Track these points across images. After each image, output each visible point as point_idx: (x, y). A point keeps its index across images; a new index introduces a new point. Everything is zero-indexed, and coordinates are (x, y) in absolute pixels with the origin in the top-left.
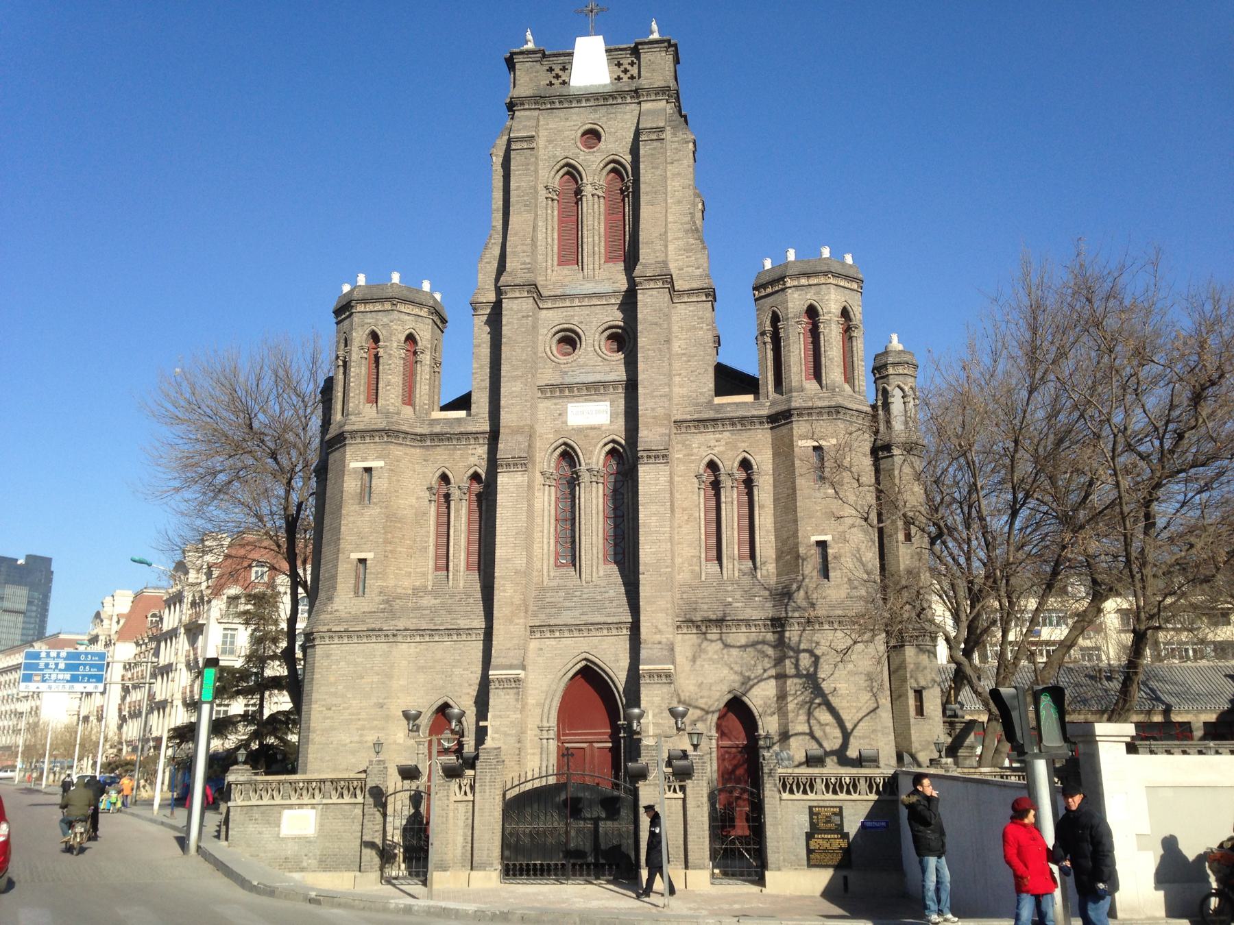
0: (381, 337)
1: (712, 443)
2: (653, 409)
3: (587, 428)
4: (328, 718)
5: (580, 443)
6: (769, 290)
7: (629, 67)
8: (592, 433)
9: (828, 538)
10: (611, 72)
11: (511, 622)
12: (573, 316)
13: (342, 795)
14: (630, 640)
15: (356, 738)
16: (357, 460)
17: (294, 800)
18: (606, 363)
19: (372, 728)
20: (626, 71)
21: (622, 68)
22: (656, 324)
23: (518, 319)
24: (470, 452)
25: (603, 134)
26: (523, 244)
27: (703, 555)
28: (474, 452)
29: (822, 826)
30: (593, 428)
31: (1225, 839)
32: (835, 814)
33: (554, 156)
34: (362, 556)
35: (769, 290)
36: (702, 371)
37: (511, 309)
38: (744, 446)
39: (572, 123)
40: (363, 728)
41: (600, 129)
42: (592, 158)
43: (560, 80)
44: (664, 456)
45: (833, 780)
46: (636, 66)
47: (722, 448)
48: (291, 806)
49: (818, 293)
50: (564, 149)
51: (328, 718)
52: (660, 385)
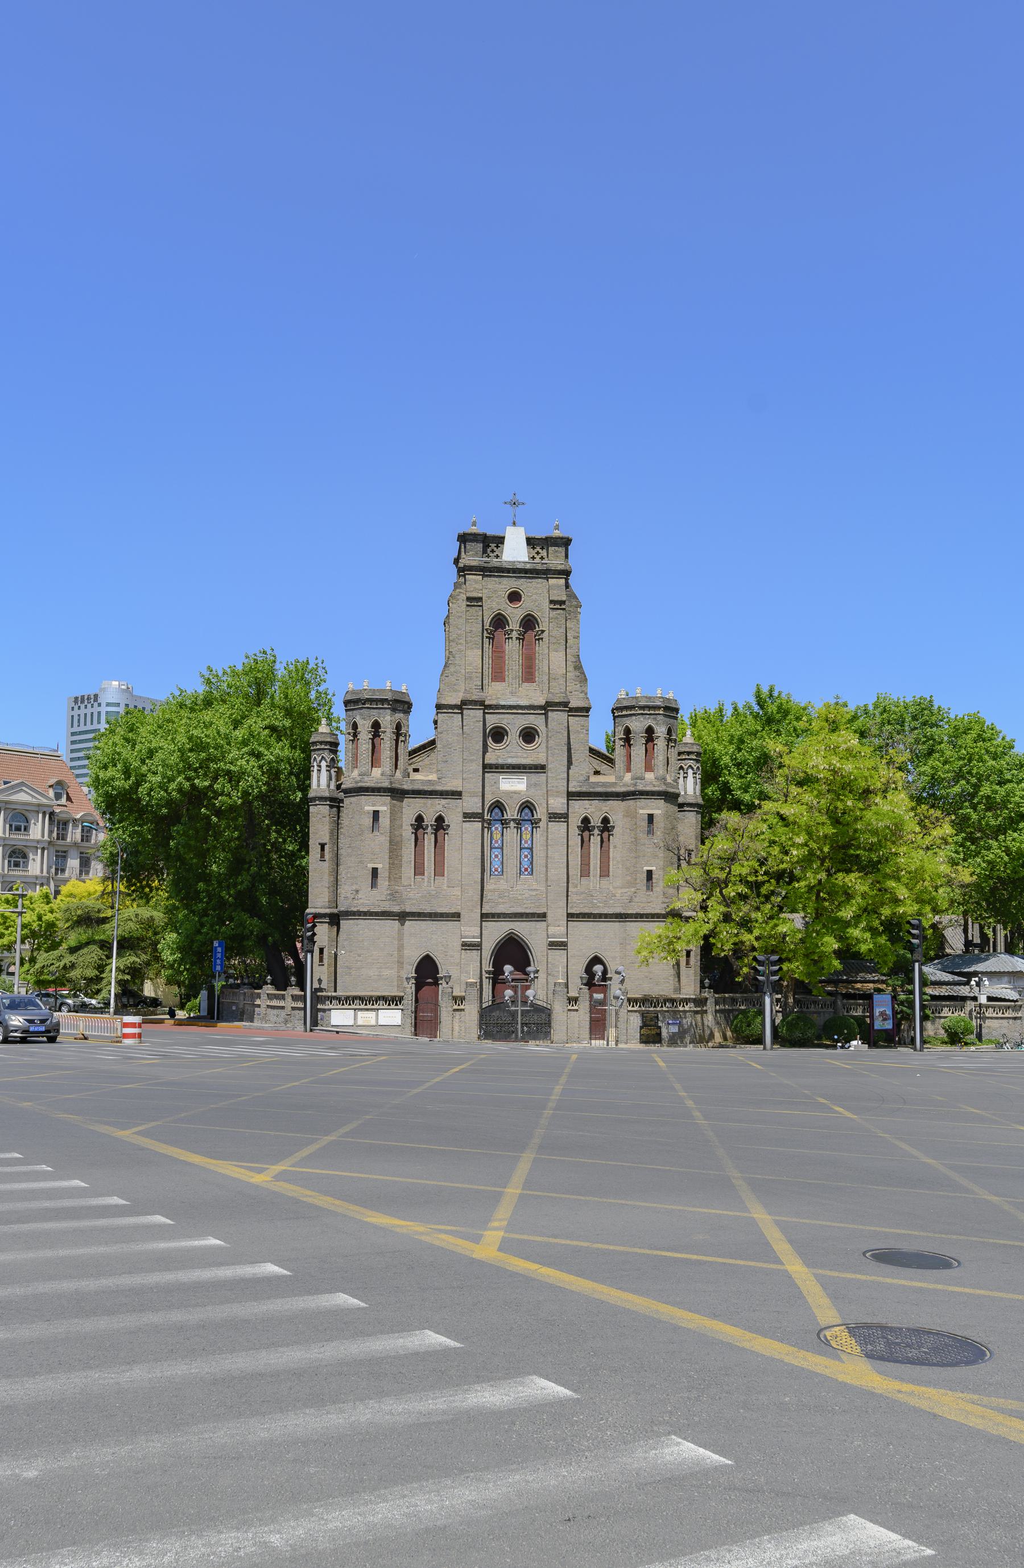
0: (382, 725)
1: (587, 807)
2: (557, 787)
3: (512, 792)
4: (359, 961)
5: (508, 802)
6: (624, 713)
7: (540, 551)
8: (515, 796)
9: (653, 868)
10: (529, 553)
11: (472, 910)
12: (503, 719)
13: (389, 1005)
14: (307, 902)
15: (376, 973)
16: (369, 806)
17: (362, 1006)
18: (524, 751)
19: (386, 968)
20: (538, 553)
21: (536, 551)
22: (559, 732)
23: (474, 722)
24: (437, 802)
25: (523, 596)
26: (476, 672)
27: (579, 874)
28: (439, 802)
29: (648, 1023)
30: (515, 792)
31: (580, 645)
32: (655, 1017)
33: (492, 608)
34: (375, 866)
35: (624, 713)
36: (582, 760)
37: (469, 715)
38: (605, 809)
39: (503, 586)
40: (381, 968)
41: (521, 592)
42: (515, 611)
43: (495, 554)
44: (565, 818)
45: (655, 1001)
46: (545, 550)
47: (593, 810)
48: (361, 1009)
49: (655, 719)
50: (498, 603)
51: (359, 961)
52: (562, 772)
